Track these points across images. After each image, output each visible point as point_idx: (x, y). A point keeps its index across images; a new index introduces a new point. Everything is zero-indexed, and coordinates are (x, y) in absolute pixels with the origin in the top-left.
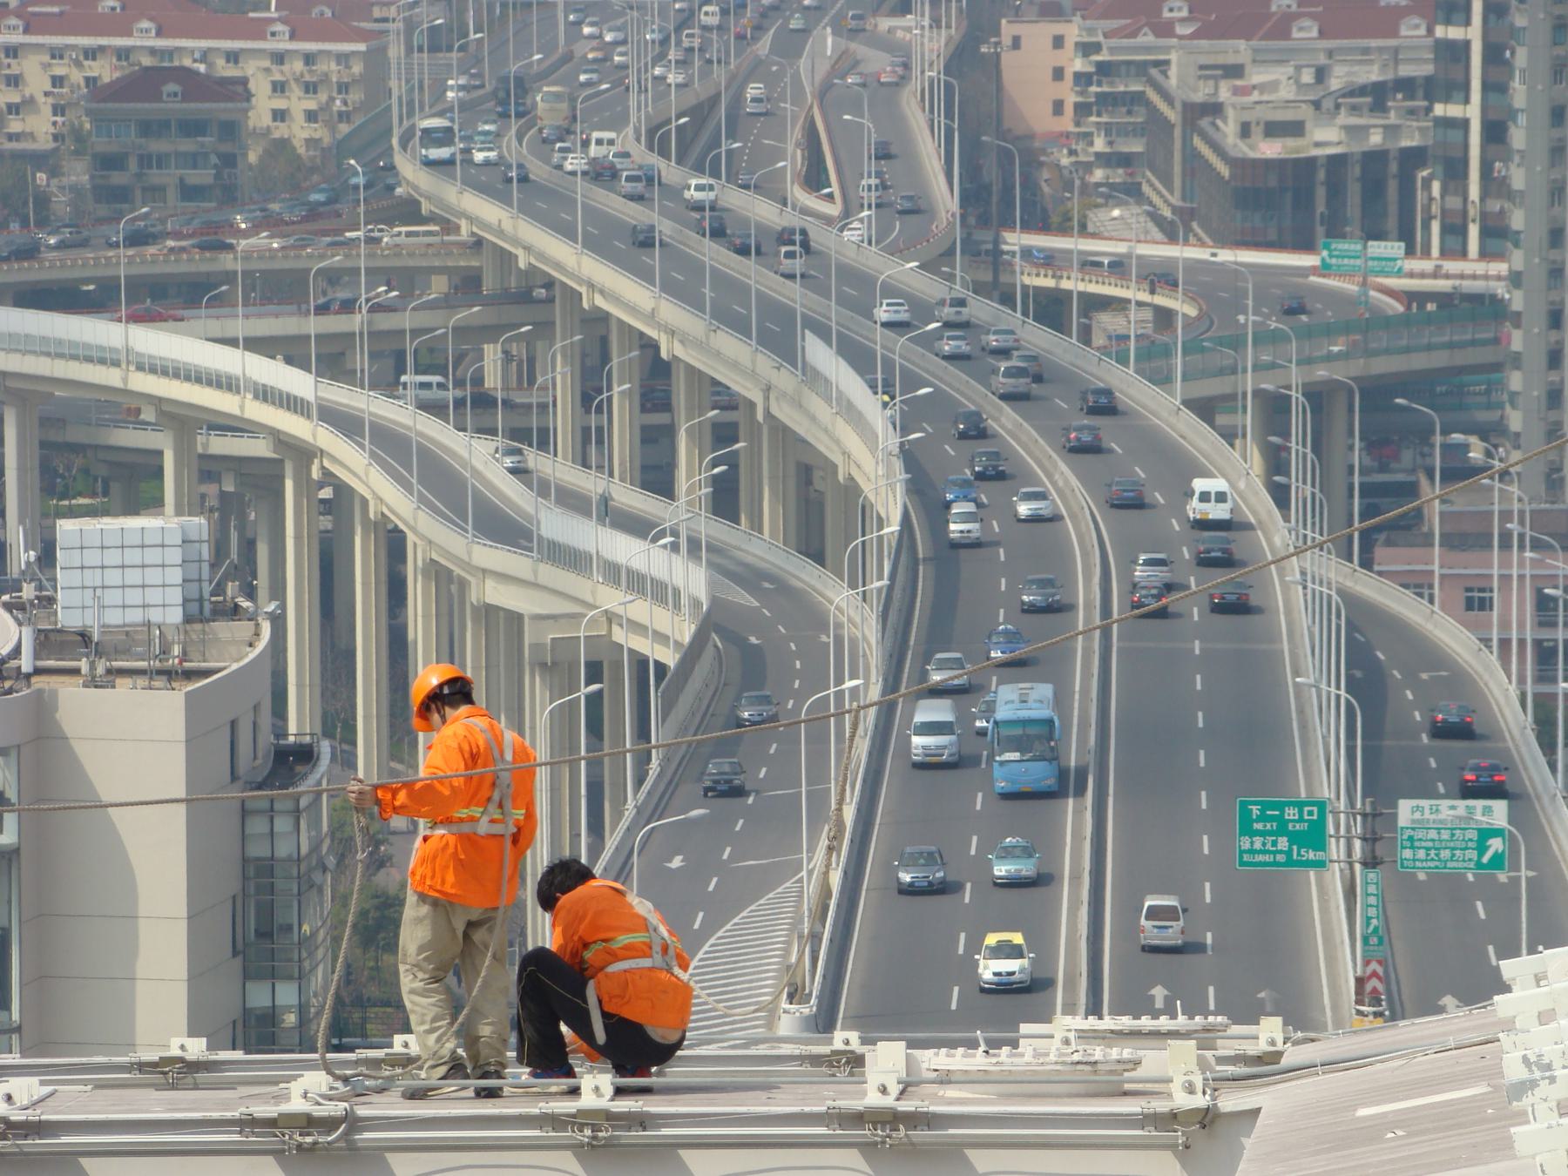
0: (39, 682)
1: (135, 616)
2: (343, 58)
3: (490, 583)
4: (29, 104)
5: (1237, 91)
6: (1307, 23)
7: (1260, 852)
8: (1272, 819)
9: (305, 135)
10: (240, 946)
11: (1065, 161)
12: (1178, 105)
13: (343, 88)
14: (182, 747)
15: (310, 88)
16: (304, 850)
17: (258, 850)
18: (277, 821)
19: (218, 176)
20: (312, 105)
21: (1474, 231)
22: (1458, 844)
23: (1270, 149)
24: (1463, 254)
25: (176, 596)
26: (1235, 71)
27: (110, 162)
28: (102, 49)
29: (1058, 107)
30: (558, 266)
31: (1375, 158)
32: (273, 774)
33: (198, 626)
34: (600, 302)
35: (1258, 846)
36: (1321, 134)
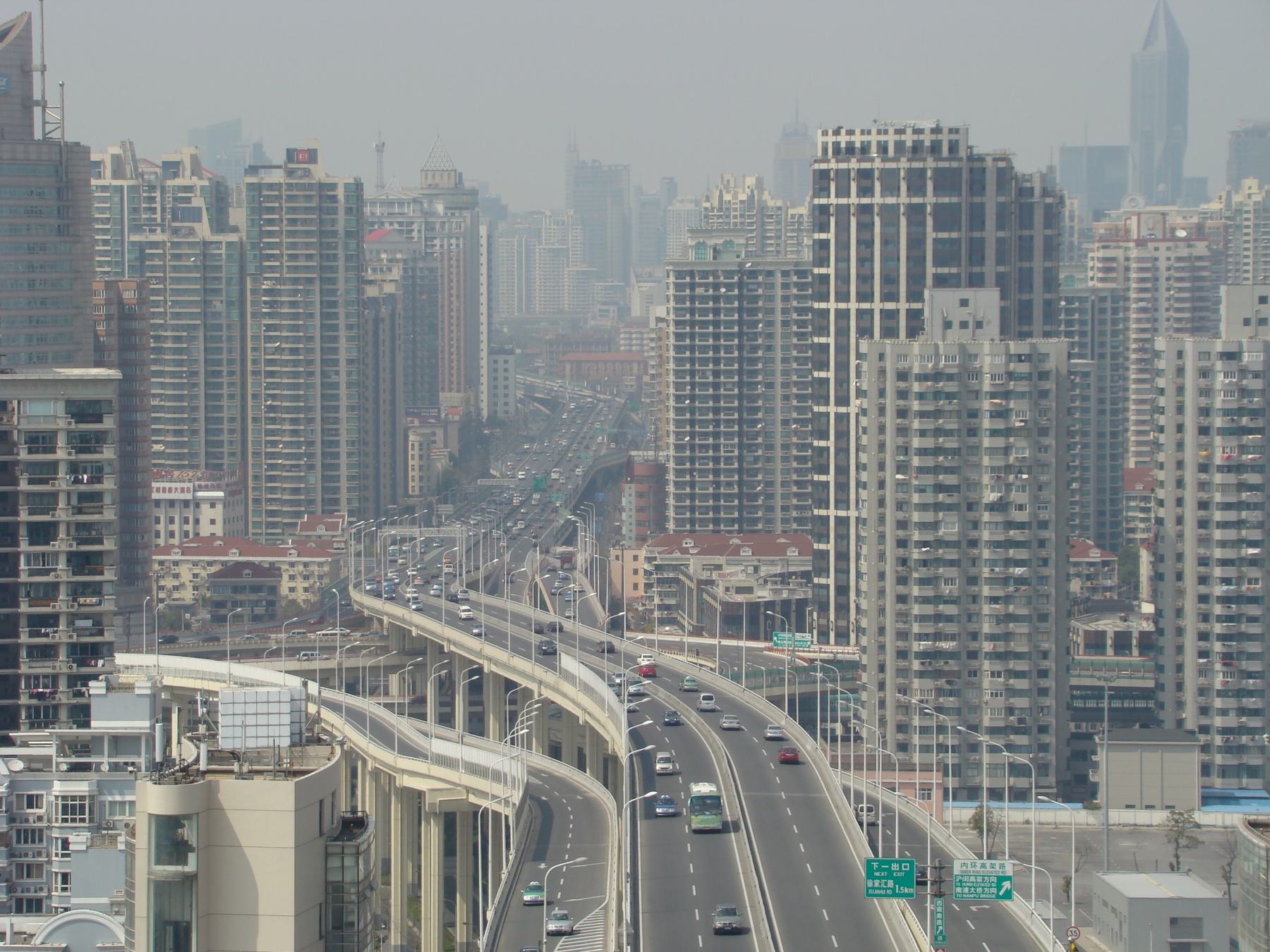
0: (209, 777)
1: (263, 743)
2: (320, 564)
3: (406, 777)
4: (182, 585)
5: (720, 575)
6: (747, 549)
7: (878, 888)
8: (885, 870)
9: (304, 598)
10: (323, 933)
11: (640, 608)
12: (695, 581)
13: (321, 577)
14: (292, 815)
15: (306, 578)
16: (361, 877)
17: (334, 877)
18: (345, 859)
19: (267, 610)
20: (306, 585)
21: (832, 634)
22: (987, 885)
23: (740, 598)
24: (828, 643)
25: (286, 731)
26: (719, 567)
27: (220, 605)
28: (215, 561)
29: (636, 586)
30: (432, 633)
31: (786, 603)
32: (341, 833)
33: (299, 749)
34: (453, 648)
35: (877, 885)
36: (760, 593)
